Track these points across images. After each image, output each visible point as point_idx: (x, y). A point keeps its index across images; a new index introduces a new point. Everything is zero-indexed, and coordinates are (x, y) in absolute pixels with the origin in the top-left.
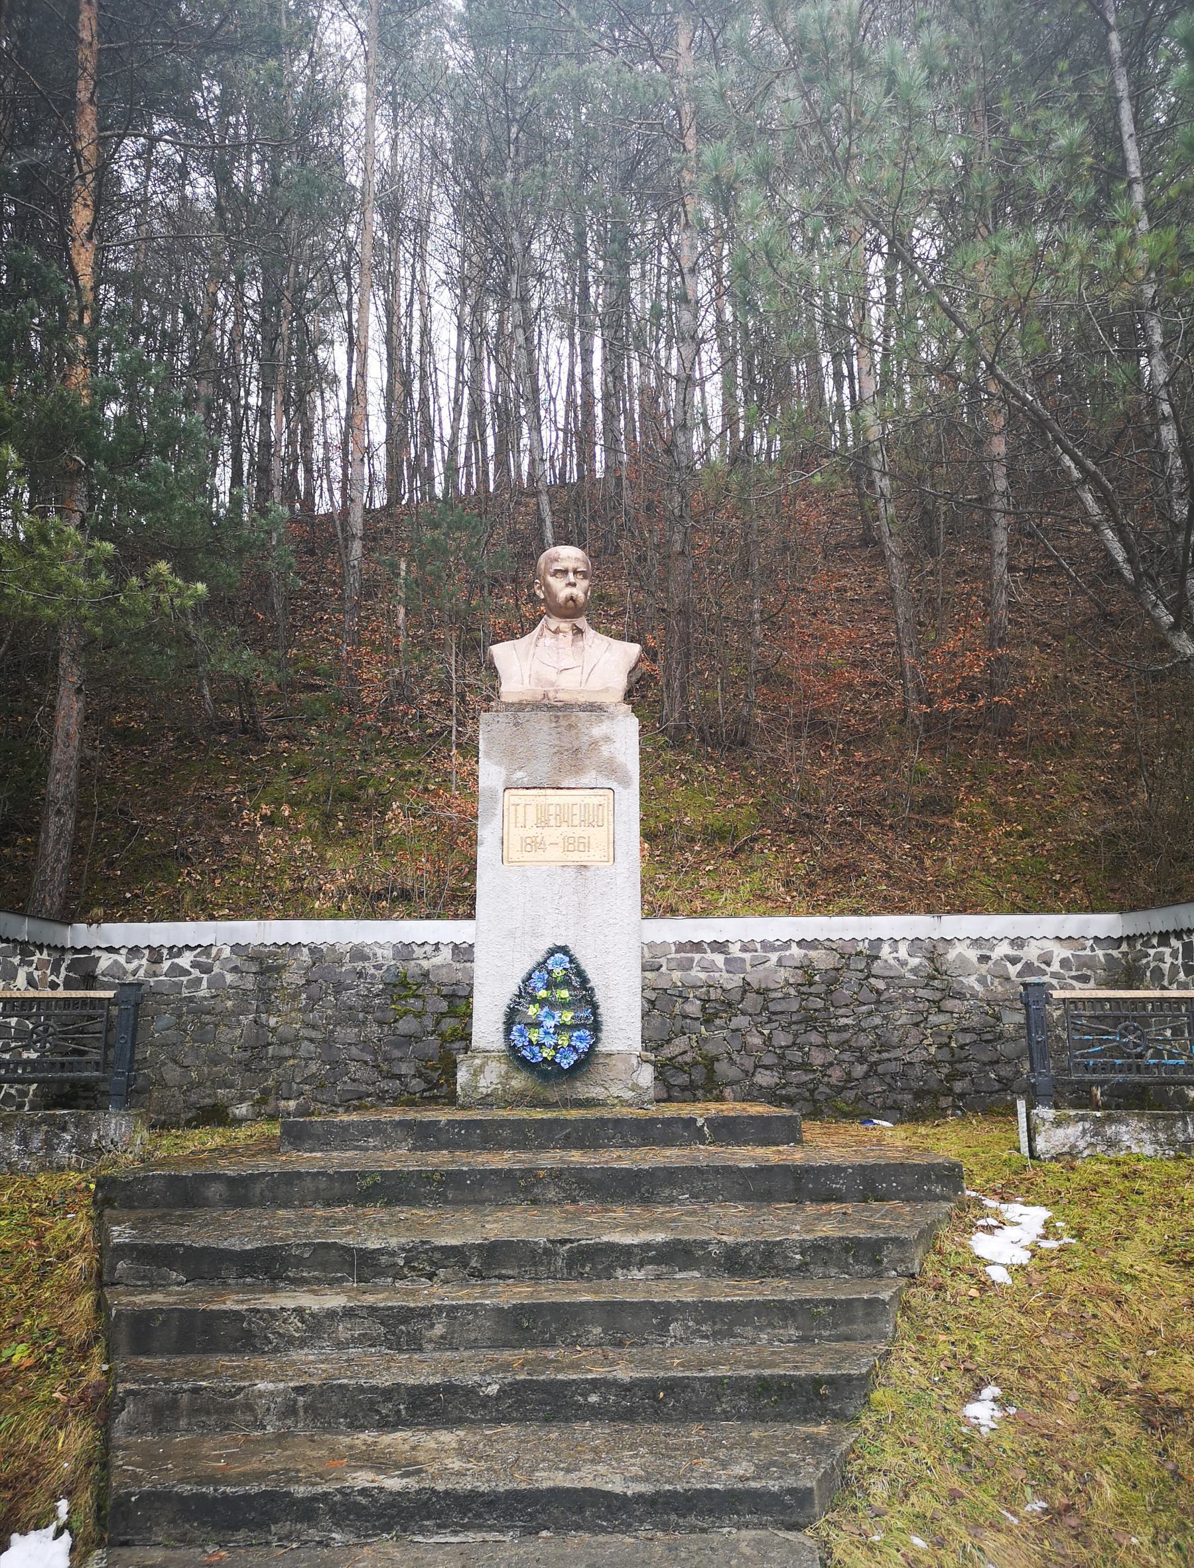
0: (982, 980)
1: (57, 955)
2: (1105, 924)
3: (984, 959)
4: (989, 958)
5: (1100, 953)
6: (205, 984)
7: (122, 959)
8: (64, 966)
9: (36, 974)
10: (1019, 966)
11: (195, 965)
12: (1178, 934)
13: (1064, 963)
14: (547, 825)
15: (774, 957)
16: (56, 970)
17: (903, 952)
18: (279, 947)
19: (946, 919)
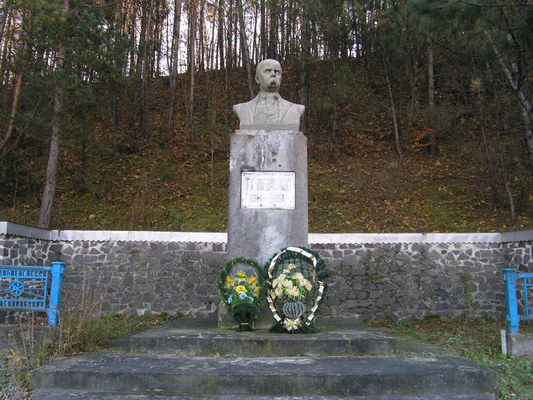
0: (443, 261)
1: (45, 243)
2: (491, 237)
3: (444, 252)
4: (446, 252)
5: (491, 250)
6: (106, 257)
7: (72, 246)
8: (49, 248)
9: (36, 251)
10: (458, 255)
11: (102, 249)
12: (530, 242)
13: (477, 254)
14: (262, 189)
15: (354, 251)
16: (45, 250)
17: (410, 249)
18: (138, 243)
19: (429, 235)
